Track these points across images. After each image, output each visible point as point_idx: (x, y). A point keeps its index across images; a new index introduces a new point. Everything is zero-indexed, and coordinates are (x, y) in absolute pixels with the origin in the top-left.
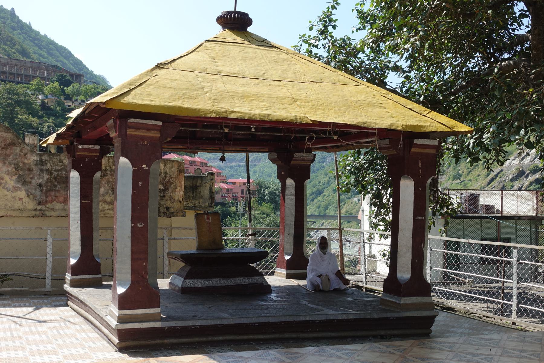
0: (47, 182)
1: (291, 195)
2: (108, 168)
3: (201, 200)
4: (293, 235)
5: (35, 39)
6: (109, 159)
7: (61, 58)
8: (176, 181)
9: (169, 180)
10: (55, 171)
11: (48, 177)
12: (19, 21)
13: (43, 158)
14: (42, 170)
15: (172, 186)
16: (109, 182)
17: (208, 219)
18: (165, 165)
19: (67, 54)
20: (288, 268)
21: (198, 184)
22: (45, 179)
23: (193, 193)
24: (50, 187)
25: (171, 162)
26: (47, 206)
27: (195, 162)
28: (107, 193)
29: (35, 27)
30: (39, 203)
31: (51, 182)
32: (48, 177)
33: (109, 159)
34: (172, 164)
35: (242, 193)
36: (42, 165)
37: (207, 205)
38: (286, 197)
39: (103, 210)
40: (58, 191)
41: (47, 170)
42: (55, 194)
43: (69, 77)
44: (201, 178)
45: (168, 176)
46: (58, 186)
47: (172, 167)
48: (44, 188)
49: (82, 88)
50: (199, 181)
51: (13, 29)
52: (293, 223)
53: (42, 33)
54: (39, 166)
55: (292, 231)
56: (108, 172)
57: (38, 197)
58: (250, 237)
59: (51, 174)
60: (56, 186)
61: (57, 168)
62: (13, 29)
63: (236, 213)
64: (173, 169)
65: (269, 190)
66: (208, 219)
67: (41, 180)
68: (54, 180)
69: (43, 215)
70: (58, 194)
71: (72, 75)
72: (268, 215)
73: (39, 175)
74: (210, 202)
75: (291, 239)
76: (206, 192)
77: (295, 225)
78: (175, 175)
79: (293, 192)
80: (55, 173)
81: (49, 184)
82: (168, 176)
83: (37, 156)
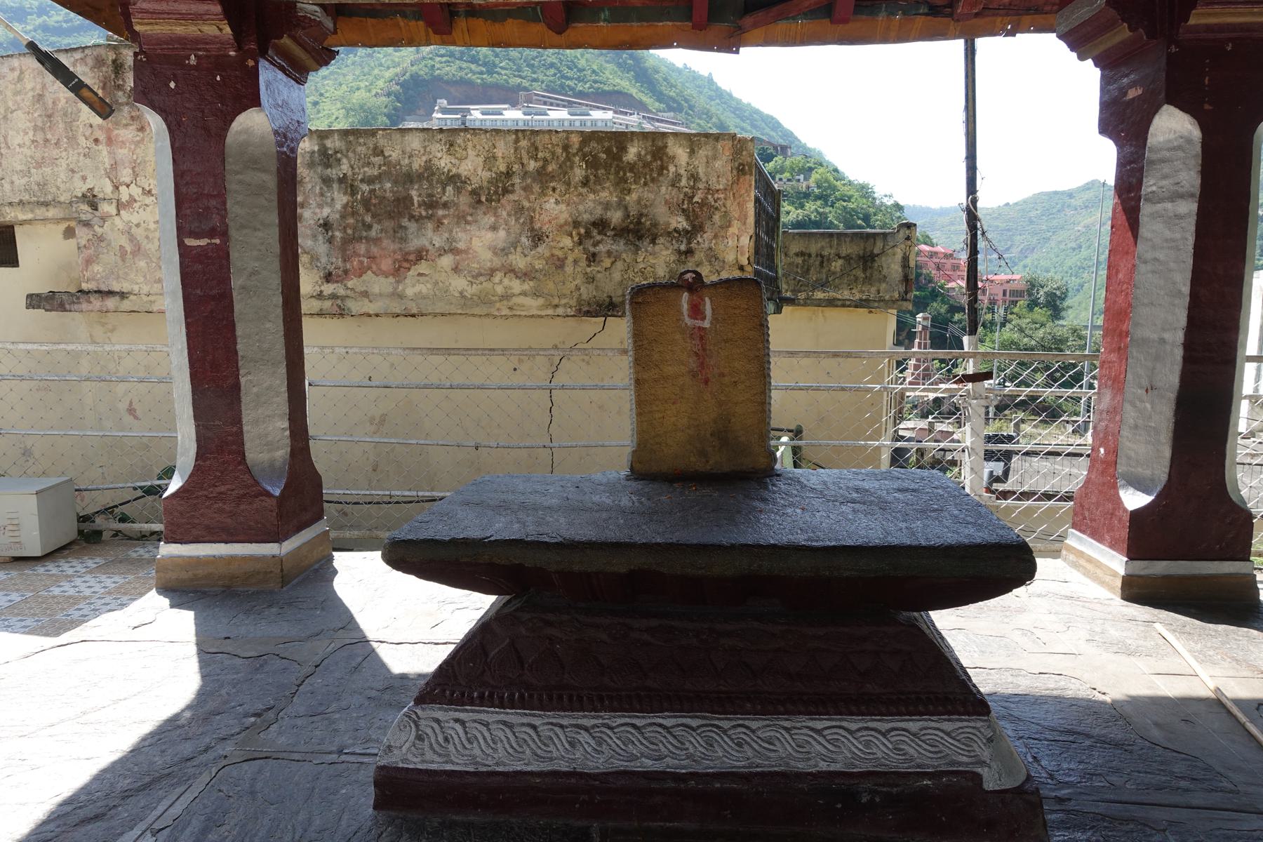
0: (343, 217)
1: (1175, 196)
2: (516, 167)
3: (884, 285)
4: (1172, 396)
5: (737, 109)
6: (517, 141)
7: (767, 130)
8: (728, 203)
9: (704, 199)
10: (362, 181)
11: (345, 199)
12: (718, 89)
13: (329, 143)
14: (327, 181)
15: (716, 218)
16: (519, 210)
17: (696, 311)
18: (692, 152)
19: (776, 125)
20: (1135, 551)
21: (876, 252)
22: (338, 206)
23: (865, 270)
24: (355, 229)
25: (711, 141)
26: (350, 284)
27: (936, 253)
28: (515, 244)
29: (735, 95)
30: (328, 278)
31: (353, 214)
32: (345, 199)
33: (517, 141)
34: (715, 148)
35: (1004, 294)
36: (328, 166)
37: (896, 295)
38: (1146, 209)
39: (506, 297)
40: (377, 241)
41: (342, 180)
42: (368, 251)
43: (771, 150)
44: (885, 235)
45: (701, 186)
46: (376, 227)
47: (715, 158)
48: (338, 234)
49: (788, 163)
50: (879, 244)
51: (711, 98)
52: (1180, 336)
53: (745, 101)
54: (319, 169)
55: (1170, 376)
56: (517, 180)
57: (324, 260)
58: (970, 385)
59: (353, 190)
60: (370, 227)
61: (370, 171)
62: (711, 98)
63: (992, 323)
64: (718, 164)
65: (1046, 289)
66: (696, 311)
67: (326, 211)
68: (362, 210)
69: (342, 313)
70: (375, 250)
71: (775, 148)
72: (1042, 325)
73: (322, 195)
74: (902, 289)
75: (1162, 415)
76: (892, 267)
77: (1188, 346)
78: (723, 181)
79: (1190, 179)
80: (365, 187)
81: (351, 221)
82: (701, 186)
83: (310, 139)
